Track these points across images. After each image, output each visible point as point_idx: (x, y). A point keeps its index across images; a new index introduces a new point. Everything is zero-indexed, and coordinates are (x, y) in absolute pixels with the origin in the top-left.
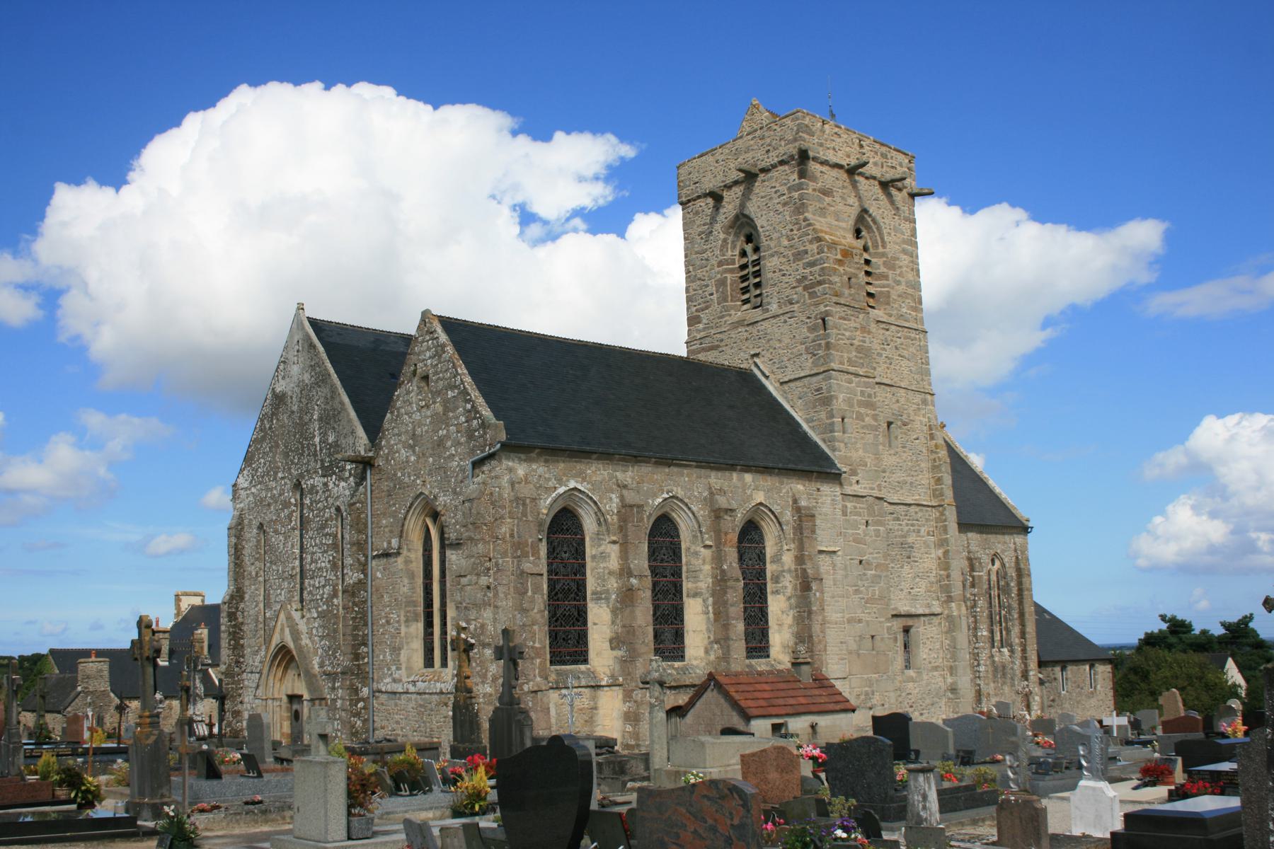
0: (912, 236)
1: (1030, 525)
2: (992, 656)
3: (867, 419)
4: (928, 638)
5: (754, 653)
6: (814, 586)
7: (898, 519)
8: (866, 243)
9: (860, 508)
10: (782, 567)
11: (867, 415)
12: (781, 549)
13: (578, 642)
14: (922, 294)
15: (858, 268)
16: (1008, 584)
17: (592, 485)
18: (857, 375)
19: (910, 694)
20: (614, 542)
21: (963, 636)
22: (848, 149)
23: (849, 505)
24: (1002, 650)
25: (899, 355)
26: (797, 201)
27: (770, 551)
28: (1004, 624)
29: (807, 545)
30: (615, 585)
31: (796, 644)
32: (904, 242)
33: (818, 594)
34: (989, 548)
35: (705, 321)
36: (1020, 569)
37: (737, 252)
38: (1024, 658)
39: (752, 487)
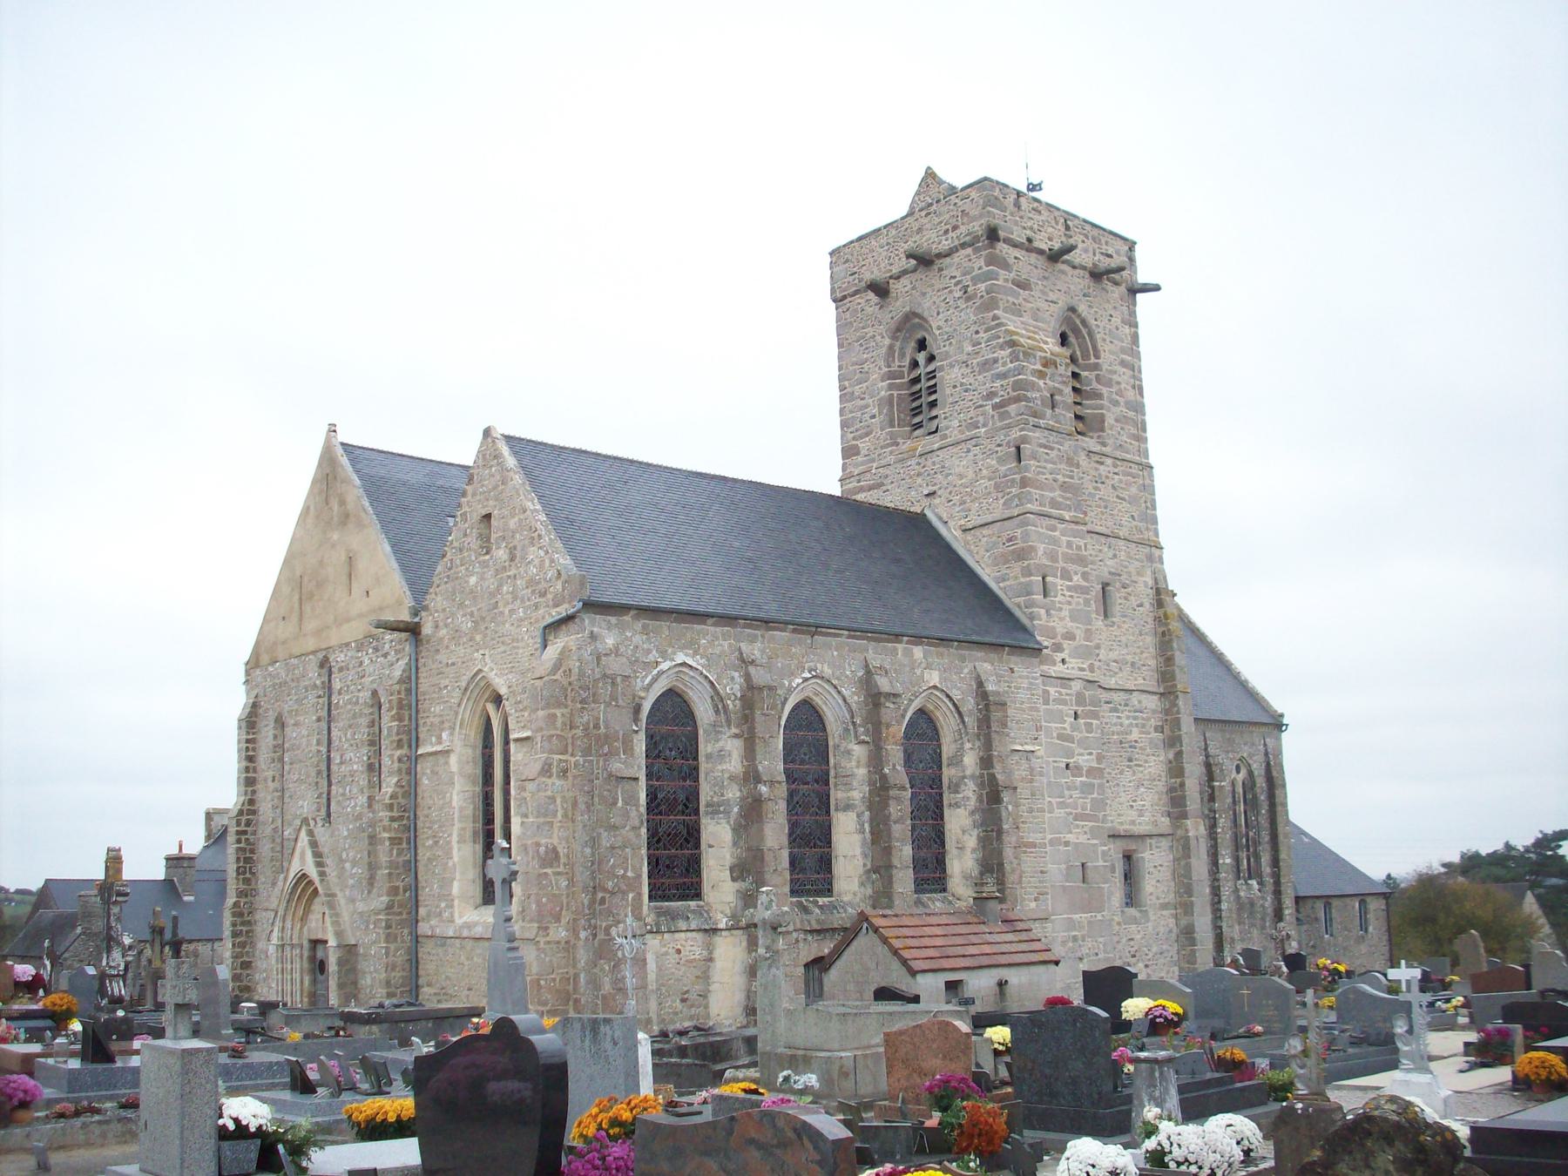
1: (1285, 722)
2: (1236, 890)
3: (1075, 578)
4: (1155, 867)
6: (1006, 797)
8: (1074, 352)
9: (1067, 694)
11: (1076, 573)
15: (1064, 382)
16: (1255, 797)
18: (1062, 520)
19: (1132, 939)
20: (736, 736)
21: (1200, 866)
22: (1050, 230)
23: (1052, 690)
24: (1250, 882)
25: (1118, 497)
26: (984, 294)
27: (947, 750)
28: (1251, 850)
29: (995, 743)
30: (738, 794)
31: (982, 874)
32: (1123, 351)
33: (1010, 807)
34: (1233, 751)
35: (864, 452)
36: (1272, 778)
38: (1277, 893)
39: (923, 665)
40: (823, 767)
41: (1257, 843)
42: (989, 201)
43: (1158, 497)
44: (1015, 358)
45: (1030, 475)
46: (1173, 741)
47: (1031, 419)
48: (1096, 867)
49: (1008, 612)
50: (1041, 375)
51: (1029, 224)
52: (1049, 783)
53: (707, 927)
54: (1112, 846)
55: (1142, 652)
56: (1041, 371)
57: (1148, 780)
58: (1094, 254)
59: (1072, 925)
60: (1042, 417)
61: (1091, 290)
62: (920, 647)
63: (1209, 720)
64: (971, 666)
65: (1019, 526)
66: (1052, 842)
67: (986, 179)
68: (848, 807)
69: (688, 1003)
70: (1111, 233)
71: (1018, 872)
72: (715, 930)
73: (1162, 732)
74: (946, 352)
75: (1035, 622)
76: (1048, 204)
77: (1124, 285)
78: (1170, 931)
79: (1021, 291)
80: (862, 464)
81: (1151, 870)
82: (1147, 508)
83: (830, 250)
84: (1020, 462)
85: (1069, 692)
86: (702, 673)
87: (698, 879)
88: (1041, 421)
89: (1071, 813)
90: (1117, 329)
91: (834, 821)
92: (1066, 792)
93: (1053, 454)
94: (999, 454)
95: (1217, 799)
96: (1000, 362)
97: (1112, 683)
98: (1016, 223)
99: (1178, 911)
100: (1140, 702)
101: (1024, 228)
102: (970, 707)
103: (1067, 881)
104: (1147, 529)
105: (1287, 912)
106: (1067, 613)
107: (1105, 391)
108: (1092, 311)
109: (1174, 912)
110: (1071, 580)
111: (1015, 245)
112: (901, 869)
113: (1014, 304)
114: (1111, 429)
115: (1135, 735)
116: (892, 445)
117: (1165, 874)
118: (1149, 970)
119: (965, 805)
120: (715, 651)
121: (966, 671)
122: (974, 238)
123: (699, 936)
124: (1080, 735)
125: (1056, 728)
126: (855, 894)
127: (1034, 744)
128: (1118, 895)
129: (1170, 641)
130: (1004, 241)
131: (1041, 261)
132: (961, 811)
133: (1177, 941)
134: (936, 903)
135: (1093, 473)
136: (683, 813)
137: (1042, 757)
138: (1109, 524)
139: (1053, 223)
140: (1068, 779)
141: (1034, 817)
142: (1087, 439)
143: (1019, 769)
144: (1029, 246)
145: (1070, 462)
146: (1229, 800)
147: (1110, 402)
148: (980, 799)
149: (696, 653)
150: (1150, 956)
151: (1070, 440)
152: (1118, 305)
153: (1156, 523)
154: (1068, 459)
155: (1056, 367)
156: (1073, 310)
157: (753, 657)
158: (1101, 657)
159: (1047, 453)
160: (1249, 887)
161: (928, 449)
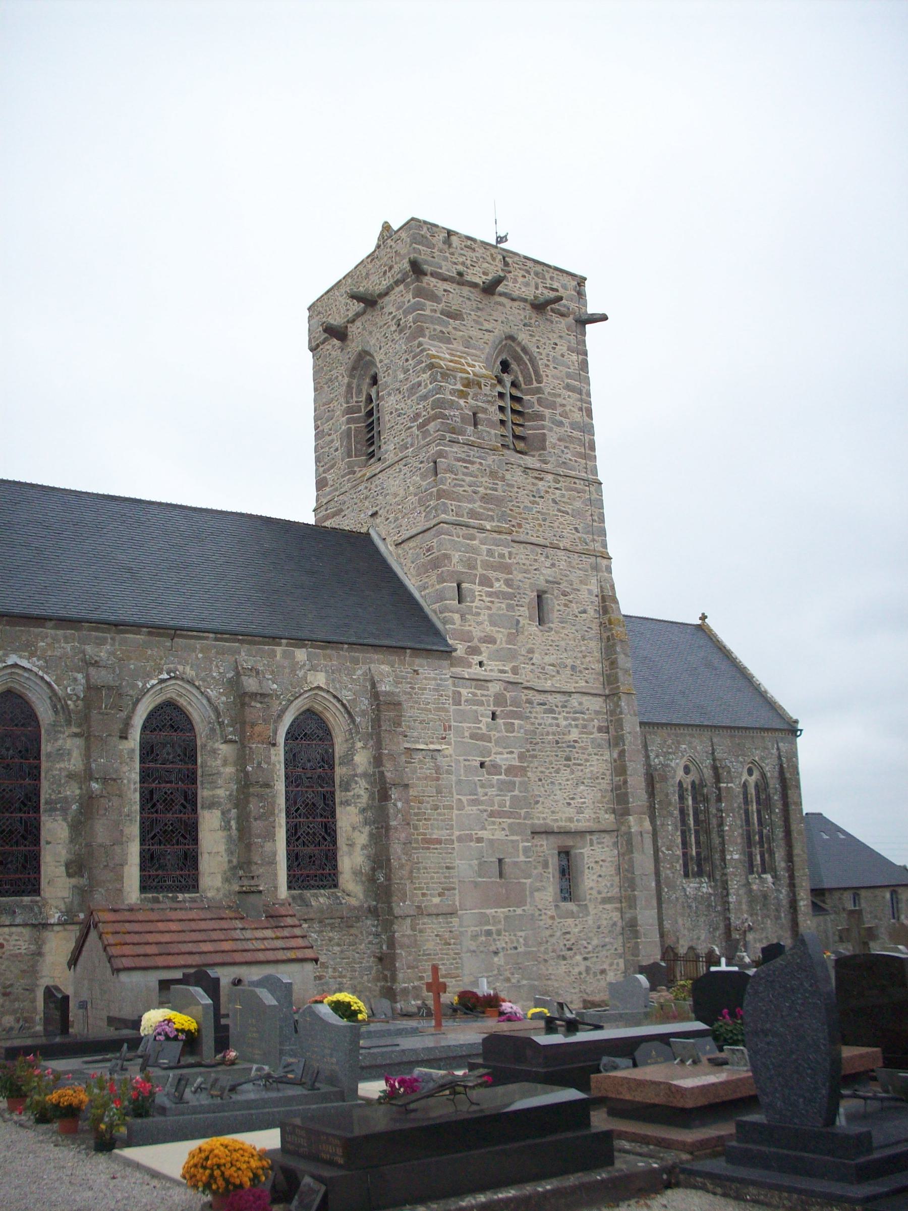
0: (582, 370)
1: (800, 727)
2: (748, 884)
3: (497, 585)
4: (596, 862)
5: (312, 882)
6: (394, 794)
7: (552, 711)
8: (517, 377)
9: (482, 695)
10: (354, 770)
11: (498, 580)
12: (353, 747)
13: (24, 867)
14: (596, 438)
15: (489, 402)
16: (769, 798)
17: (46, 662)
18: (482, 529)
19: (568, 933)
20: (76, 735)
21: (644, 862)
22: (485, 265)
23: (464, 692)
24: (764, 876)
25: (559, 510)
27: (339, 749)
28: (766, 846)
29: (386, 741)
30: (78, 792)
31: (373, 869)
32: (569, 376)
33: (399, 804)
34: (743, 755)
35: (330, 483)
36: (785, 779)
37: (363, 398)
38: (792, 886)
39: (307, 667)
40: (190, 766)
41: (770, 840)
42: (415, 238)
43: (606, 511)
44: (433, 379)
45: (445, 487)
46: (617, 741)
47: (448, 435)
48: (515, 863)
49: (425, 618)
50: (463, 395)
51: (461, 260)
52: (459, 782)
53: (34, 922)
54: (545, 843)
55: (584, 657)
56: (462, 391)
57: (591, 778)
58: (537, 288)
59: (483, 919)
60: (462, 433)
61: (533, 321)
62: (304, 650)
63: (715, 727)
64: (365, 668)
65: (435, 536)
66: (460, 839)
67: (413, 219)
68: (211, 805)
69: (12, 997)
70: (556, 269)
71: (408, 868)
72: (45, 926)
73: (608, 732)
74: (386, 382)
75: (447, 627)
76: (483, 242)
77: (572, 316)
78: (615, 924)
79: (451, 321)
80: (329, 494)
81: (591, 865)
82: (593, 521)
83: (308, 306)
84: (436, 474)
85: (485, 693)
86: (37, 674)
87: (36, 875)
88: (460, 437)
89: (486, 811)
90: (563, 356)
91: (200, 820)
92: (479, 790)
93: (473, 468)
94: (422, 470)
95: (723, 799)
96: (423, 384)
97: (548, 685)
98: (446, 259)
99: (624, 905)
100: (580, 704)
101: (455, 264)
102: (364, 707)
103: (480, 876)
104: (593, 540)
105: (802, 903)
106: (486, 617)
107: (547, 412)
108: (534, 340)
109: (618, 905)
110: (492, 587)
111: (445, 279)
112: (262, 865)
113: (442, 332)
114: (554, 448)
115: (574, 735)
116: (349, 473)
117: (609, 869)
118: (588, 963)
119: (355, 803)
120: (55, 653)
121: (359, 672)
122: (404, 274)
123: (25, 931)
124: (498, 735)
125: (470, 728)
126: (218, 890)
127: (441, 743)
128: (551, 889)
129: (614, 645)
130: (432, 275)
131: (475, 295)
132: (352, 810)
133: (622, 934)
134: (320, 899)
135: (530, 487)
136: (20, 810)
137: (451, 756)
138: (547, 535)
139: (489, 259)
140: (483, 776)
141: (439, 814)
142: (527, 457)
143: (421, 768)
144: (460, 279)
145: (493, 474)
146: (741, 799)
147: (553, 423)
148: (372, 797)
149: (32, 655)
150: (590, 948)
151: (494, 455)
152: (563, 334)
153: (605, 535)
154: (491, 472)
155: (480, 388)
156: (511, 338)
157: (97, 659)
158: (534, 661)
159: (465, 467)
160: (763, 881)
161: (374, 473)
